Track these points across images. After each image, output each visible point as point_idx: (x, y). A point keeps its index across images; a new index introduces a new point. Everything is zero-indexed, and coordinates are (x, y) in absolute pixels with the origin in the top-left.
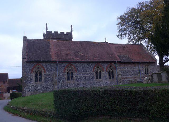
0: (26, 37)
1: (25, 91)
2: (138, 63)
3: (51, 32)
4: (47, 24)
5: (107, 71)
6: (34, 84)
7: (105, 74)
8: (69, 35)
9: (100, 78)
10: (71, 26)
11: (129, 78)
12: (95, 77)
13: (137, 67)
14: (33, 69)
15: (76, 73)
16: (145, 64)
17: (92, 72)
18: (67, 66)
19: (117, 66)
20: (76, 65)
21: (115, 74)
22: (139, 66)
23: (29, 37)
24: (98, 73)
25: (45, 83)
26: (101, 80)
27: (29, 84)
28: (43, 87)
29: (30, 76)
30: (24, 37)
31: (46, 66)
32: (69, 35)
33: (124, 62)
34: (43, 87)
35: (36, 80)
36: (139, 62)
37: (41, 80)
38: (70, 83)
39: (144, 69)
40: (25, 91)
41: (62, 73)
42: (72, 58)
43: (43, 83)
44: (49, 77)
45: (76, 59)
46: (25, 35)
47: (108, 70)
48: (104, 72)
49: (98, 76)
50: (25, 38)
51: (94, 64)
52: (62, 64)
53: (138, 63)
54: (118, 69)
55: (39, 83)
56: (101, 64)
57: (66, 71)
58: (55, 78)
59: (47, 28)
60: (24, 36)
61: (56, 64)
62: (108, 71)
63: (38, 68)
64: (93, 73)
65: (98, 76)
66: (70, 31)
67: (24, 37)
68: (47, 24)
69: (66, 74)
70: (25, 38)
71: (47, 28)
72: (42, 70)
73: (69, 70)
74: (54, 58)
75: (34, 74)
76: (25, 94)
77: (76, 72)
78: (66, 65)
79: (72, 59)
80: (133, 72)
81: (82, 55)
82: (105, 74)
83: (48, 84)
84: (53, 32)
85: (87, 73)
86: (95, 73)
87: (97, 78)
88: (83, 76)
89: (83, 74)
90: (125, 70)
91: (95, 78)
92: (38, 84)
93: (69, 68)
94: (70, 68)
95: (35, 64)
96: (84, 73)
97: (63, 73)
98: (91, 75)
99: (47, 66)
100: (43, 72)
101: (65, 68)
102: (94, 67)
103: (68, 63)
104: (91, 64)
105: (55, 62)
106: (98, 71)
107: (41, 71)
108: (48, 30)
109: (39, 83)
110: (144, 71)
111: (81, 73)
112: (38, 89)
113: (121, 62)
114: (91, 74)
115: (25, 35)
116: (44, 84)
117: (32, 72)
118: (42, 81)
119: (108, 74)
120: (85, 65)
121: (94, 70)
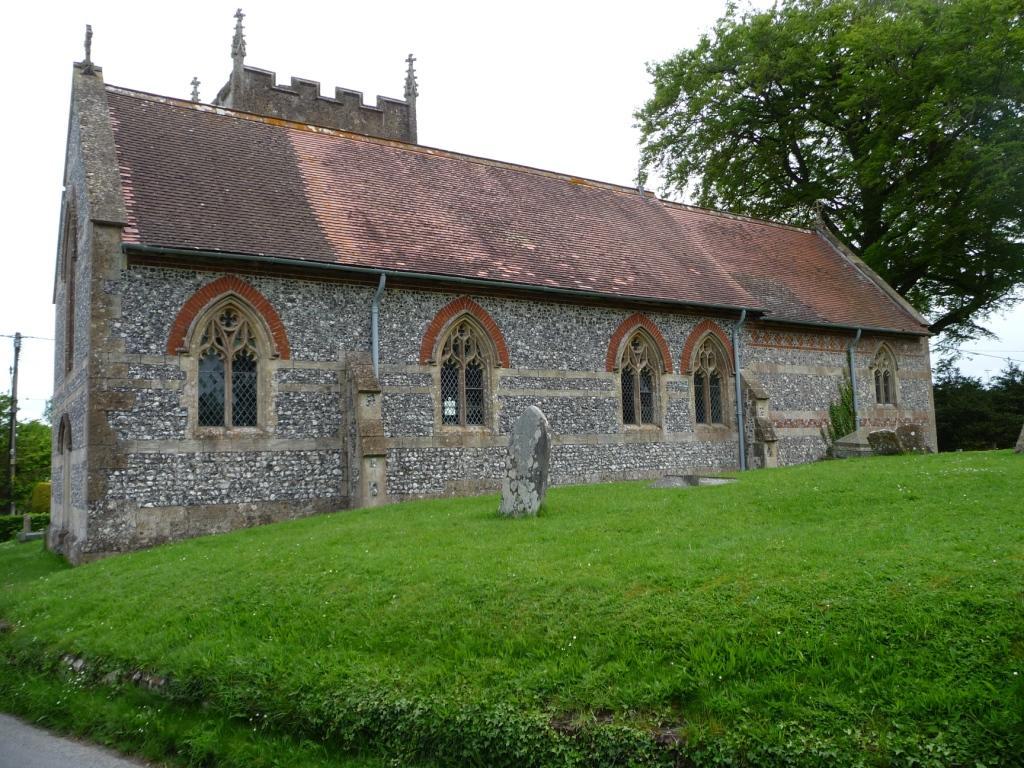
0: (100, 70)
1: (111, 506)
2: (843, 333)
3: (264, 78)
4: (239, 16)
5: (611, 367)
6: (192, 446)
7: (674, 389)
8: (397, 118)
9: (647, 418)
10: (410, 60)
11: (801, 423)
12: (621, 405)
13: (841, 359)
14: (185, 318)
15: (501, 372)
16: (880, 344)
17: (602, 374)
18: (442, 315)
19: (742, 342)
20: (503, 314)
21: (730, 394)
22: (849, 353)
23: (114, 76)
24: (462, 373)
25: (282, 436)
26: (649, 427)
27: (151, 446)
28: (270, 467)
29: (162, 373)
30: (77, 66)
31: (292, 301)
32: (397, 118)
33: (781, 319)
34: (270, 467)
35: (210, 414)
36: (851, 325)
37: (246, 413)
38: (461, 441)
39: (873, 371)
40: (111, 506)
41: (410, 369)
42: (470, 257)
43: (264, 436)
44: (316, 389)
45: (509, 272)
46: (88, 54)
47: (692, 362)
48: (668, 378)
49: (637, 403)
50: (87, 70)
51: (617, 317)
52: (410, 300)
53: (843, 333)
54: (746, 360)
55: (238, 436)
56: (657, 319)
57: (438, 356)
58: (364, 401)
59: (238, 49)
60: (81, 58)
61: (365, 294)
62: (621, 366)
63: (229, 317)
64: (610, 375)
65: (637, 403)
66: (398, 94)
67: (77, 66)
68: (239, 16)
69: (436, 371)
70: (87, 70)
71: (238, 49)
72: (261, 328)
73: (456, 348)
74: (349, 251)
75: (189, 364)
76: (115, 526)
77: (506, 365)
78: (434, 304)
79: (476, 266)
80: (822, 387)
81: (531, 247)
82: (674, 389)
83: (307, 445)
84: (283, 80)
85: (570, 375)
86: (618, 381)
87: (629, 418)
88: (551, 393)
89: (573, 385)
90: (781, 369)
91: (619, 415)
92: (224, 446)
93: (458, 334)
94: (462, 331)
95: (199, 278)
96: (551, 374)
97: (417, 369)
98: (595, 394)
99: (298, 304)
100: (264, 347)
101: (431, 334)
102: (616, 339)
103: (453, 297)
104: (597, 313)
105: (360, 278)
106: (639, 368)
107: (252, 341)
108: (251, 61)
109: (232, 436)
110: (872, 388)
111: (533, 374)
112: (225, 485)
113: (768, 317)
114: (594, 383)
115: (88, 54)
116: (273, 444)
117: (176, 348)
118: (252, 422)
119: (692, 390)
120: (566, 320)
121: (612, 357)
